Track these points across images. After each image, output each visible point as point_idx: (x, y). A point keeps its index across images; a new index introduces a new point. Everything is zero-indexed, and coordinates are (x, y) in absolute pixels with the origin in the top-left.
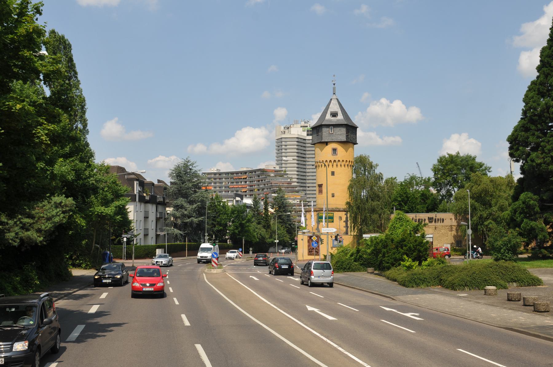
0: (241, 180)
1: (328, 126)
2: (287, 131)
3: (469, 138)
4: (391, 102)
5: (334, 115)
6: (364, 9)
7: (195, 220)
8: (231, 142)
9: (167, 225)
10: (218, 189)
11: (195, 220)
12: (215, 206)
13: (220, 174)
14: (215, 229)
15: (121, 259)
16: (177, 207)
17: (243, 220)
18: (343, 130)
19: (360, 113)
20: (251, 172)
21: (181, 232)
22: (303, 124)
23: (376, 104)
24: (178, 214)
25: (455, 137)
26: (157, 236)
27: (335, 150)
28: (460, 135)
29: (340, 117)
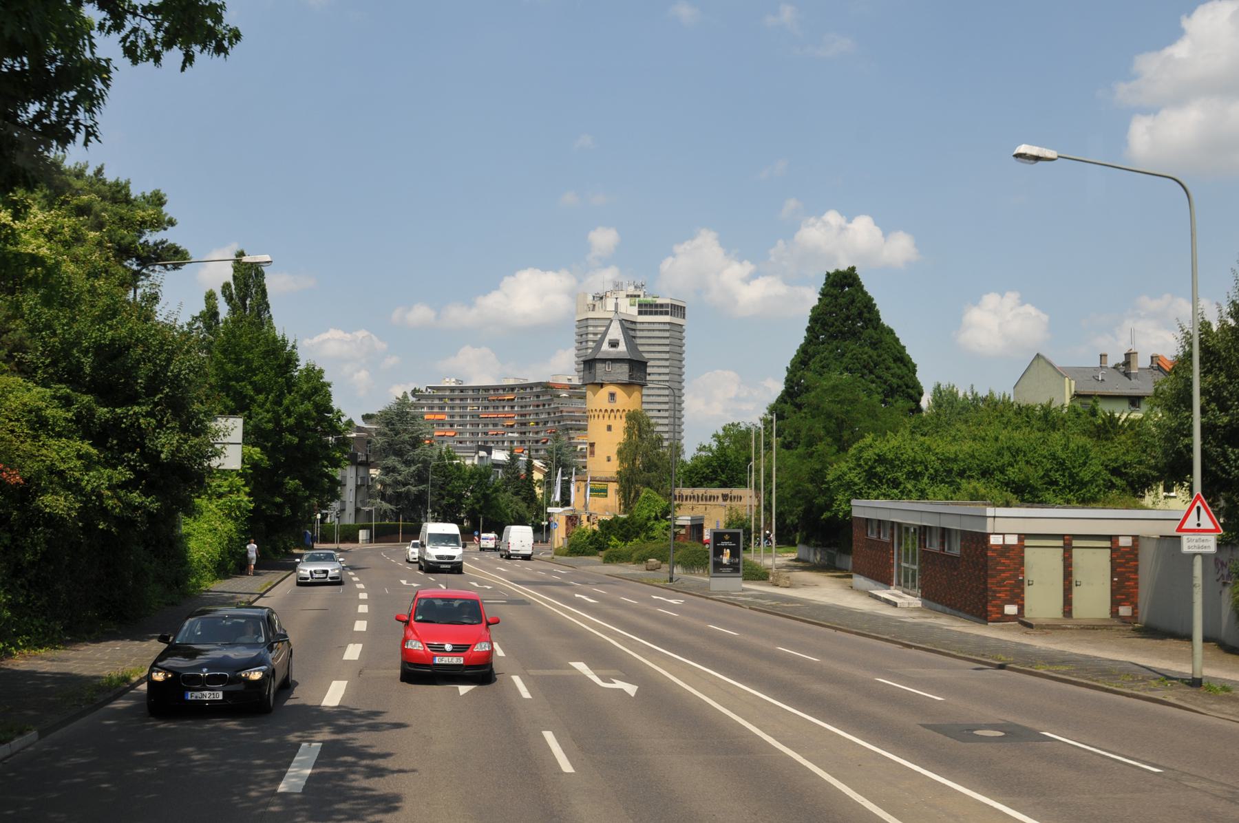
0: (503, 403)
1: (604, 361)
2: (598, 303)
3: (1023, 304)
4: (849, 221)
5: (614, 344)
6: (787, 13)
7: (413, 489)
8: (492, 302)
9: (371, 496)
10: (457, 419)
11: (413, 489)
12: (445, 466)
13: (462, 390)
14: (445, 502)
15: (333, 542)
16: (388, 470)
17: (488, 488)
18: (625, 368)
19: (780, 242)
20: (523, 387)
21: (392, 507)
22: (631, 290)
23: (813, 225)
24: (388, 480)
25: (991, 300)
26: (357, 510)
27: (612, 395)
28: (1002, 295)
29: (622, 347)
